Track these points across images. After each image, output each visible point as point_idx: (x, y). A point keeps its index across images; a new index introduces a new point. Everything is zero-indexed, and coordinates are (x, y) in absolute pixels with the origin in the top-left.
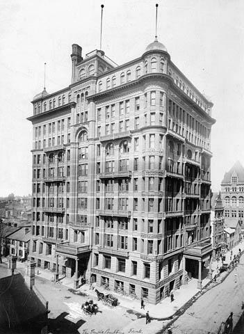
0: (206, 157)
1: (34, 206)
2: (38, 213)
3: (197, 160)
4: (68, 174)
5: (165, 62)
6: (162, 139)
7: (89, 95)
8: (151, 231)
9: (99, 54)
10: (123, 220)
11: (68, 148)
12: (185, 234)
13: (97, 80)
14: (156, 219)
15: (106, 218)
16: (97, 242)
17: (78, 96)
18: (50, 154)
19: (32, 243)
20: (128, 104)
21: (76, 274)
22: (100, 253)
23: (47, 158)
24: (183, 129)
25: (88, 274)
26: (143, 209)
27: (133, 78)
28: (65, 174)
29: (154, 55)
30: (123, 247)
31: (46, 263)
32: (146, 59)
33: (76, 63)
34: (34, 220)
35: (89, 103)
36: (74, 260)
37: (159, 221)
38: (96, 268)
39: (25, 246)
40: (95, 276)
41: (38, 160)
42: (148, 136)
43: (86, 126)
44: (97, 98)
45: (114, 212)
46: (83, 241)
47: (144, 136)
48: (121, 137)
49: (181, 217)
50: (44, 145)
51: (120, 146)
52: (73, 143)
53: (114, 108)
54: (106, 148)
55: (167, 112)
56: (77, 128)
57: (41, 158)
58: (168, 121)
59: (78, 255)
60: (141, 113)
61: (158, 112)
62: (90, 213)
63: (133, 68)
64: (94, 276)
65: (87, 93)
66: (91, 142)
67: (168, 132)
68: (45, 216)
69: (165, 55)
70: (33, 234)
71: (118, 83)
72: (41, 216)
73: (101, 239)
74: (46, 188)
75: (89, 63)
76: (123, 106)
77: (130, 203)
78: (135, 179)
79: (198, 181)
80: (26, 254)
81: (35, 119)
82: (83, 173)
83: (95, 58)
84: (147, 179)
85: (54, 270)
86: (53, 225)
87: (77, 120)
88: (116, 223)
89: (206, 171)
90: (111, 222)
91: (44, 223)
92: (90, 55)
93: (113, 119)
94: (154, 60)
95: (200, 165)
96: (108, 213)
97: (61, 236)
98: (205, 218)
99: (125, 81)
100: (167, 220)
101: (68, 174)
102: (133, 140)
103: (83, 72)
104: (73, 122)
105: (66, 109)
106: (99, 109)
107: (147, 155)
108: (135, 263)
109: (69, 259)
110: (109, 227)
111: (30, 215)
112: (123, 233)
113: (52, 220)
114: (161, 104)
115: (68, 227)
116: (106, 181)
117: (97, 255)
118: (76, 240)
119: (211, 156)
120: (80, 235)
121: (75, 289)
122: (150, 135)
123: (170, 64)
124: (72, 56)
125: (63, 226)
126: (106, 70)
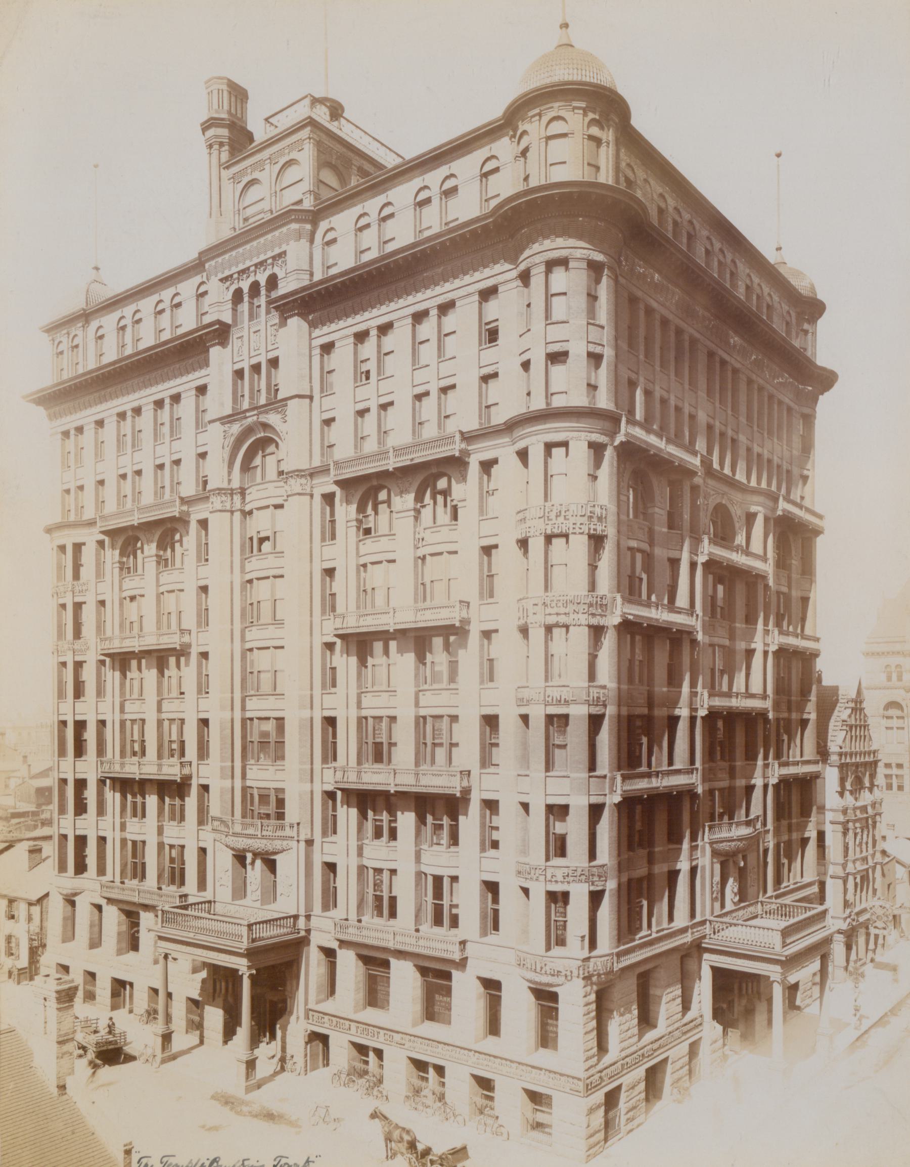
0: (794, 537)
1: (62, 752)
2: (81, 784)
3: (756, 546)
4: (203, 751)
5: (608, 135)
6: (598, 463)
7: (285, 287)
8: (562, 851)
9: (322, 115)
10: (440, 807)
11: (197, 513)
12: (705, 860)
13: (315, 223)
14: (579, 804)
15: (365, 800)
16: (330, 899)
17: (238, 296)
18: (127, 539)
19: (56, 906)
20: (450, 321)
21: (243, 1032)
22: (343, 943)
23: (112, 556)
24: (692, 417)
25: (296, 1029)
26: (525, 759)
27: (468, 207)
28: (189, 621)
29: (556, 108)
30: (438, 920)
31: (120, 986)
32: (522, 127)
33: (225, 156)
34: (62, 810)
35: (283, 322)
36: (232, 975)
37: (595, 811)
38: (329, 1006)
39: (30, 919)
40: (324, 1039)
41: (77, 567)
42: (536, 454)
43: (272, 418)
44: (323, 301)
45: (401, 773)
46: (270, 893)
47: (523, 455)
48: (420, 457)
49: (689, 793)
50: (100, 503)
51: (419, 498)
52: (220, 491)
53: (389, 341)
54: (361, 509)
55: (617, 348)
56: (236, 429)
57: (88, 555)
58: (624, 387)
59: (250, 954)
60: (504, 355)
61: (578, 350)
62: (297, 778)
63: (466, 167)
64: (320, 1039)
65: (273, 282)
66: (296, 485)
67: (625, 432)
68: (109, 794)
69: (607, 106)
70: (62, 868)
71: (402, 234)
72: (91, 794)
73: (347, 885)
74: (112, 677)
75: (281, 152)
76: (428, 329)
77: (468, 734)
78: (487, 634)
79: (765, 639)
80: (34, 953)
81: (59, 1043)
82: (266, 616)
83: (306, 133)
84: (536, 545)
85: (151, 1014)
86: (145, 829)
87: (236, 397)
88: (406, 820)
89: (791, 610)
90: (385, 816)
91: (105, 823)
92: (285, 121)
93: (385, 386)
94: (557, 128)
95: (768, 568)
96: (375, 778)
97: (177, 876)
98: (797, 797)
99: (433, 221)
100: (628, 804)
101: (203, 751)
102: (474, 469)
103: (254, 193)
104: (219, 401)
105: (189, 350)
106: (327, 348)
107: (536, 529)
108: (492, 986)
109: (215, 970)
110: (378, 834)
111: (49, 789)
112: (439, 859)
113: (140, 812)
114: (591, 312)
115: (208, 838)
116: (361, 644)
117: (329, 953)
118: (240, 891)
119: (817, 532)
120: (256, 872)
121: (240, 1093)
122: (549, 447)
123: (632, 141)
124: (206, 126)
125: (186, 834)
126: (354, 181)
